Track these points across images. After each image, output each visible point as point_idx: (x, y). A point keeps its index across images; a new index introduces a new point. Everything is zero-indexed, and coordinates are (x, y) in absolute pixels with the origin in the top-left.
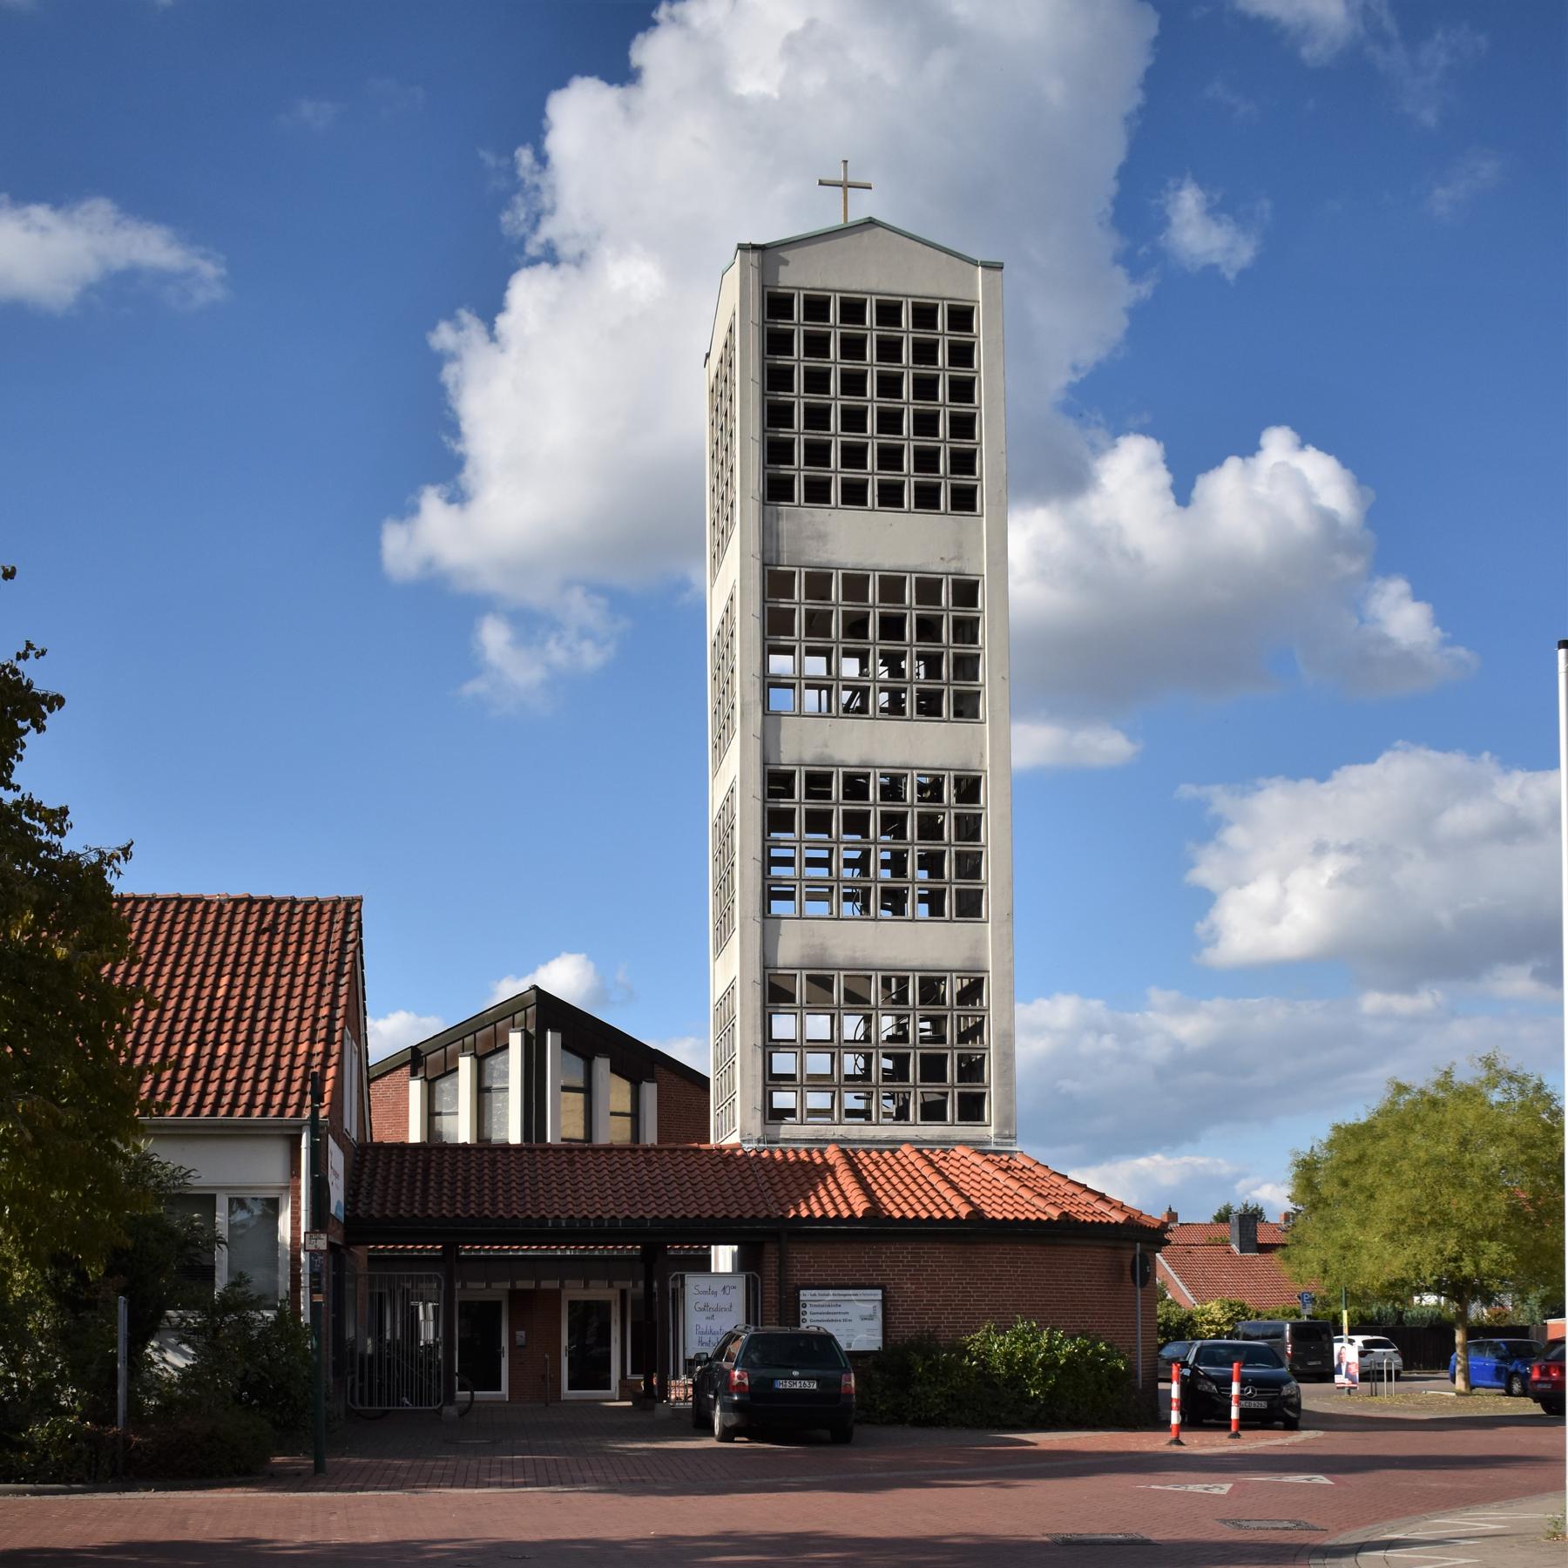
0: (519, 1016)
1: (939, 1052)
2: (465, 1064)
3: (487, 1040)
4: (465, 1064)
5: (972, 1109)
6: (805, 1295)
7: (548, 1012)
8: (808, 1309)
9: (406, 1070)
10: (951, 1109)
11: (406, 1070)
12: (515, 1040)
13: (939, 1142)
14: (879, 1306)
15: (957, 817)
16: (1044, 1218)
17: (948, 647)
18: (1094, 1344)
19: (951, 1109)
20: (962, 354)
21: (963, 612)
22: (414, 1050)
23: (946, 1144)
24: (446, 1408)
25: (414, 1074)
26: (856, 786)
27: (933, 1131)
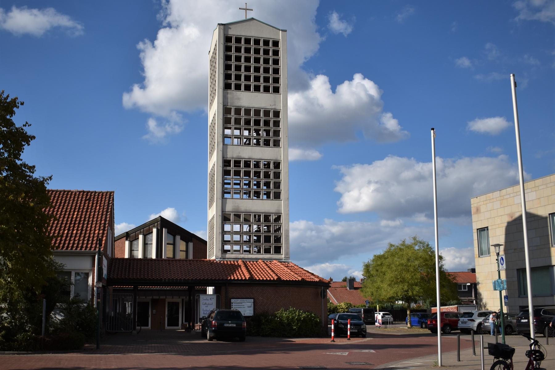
2: (141, 237)
4: (141, 237)
5: (278, 250)
7: (163, 223)
9: (125, 238)
10: (272, 250)
11: (125, 238)
19: (272, 250)
21: (276, 119)
25: (127, 239)
27: (267, 256)
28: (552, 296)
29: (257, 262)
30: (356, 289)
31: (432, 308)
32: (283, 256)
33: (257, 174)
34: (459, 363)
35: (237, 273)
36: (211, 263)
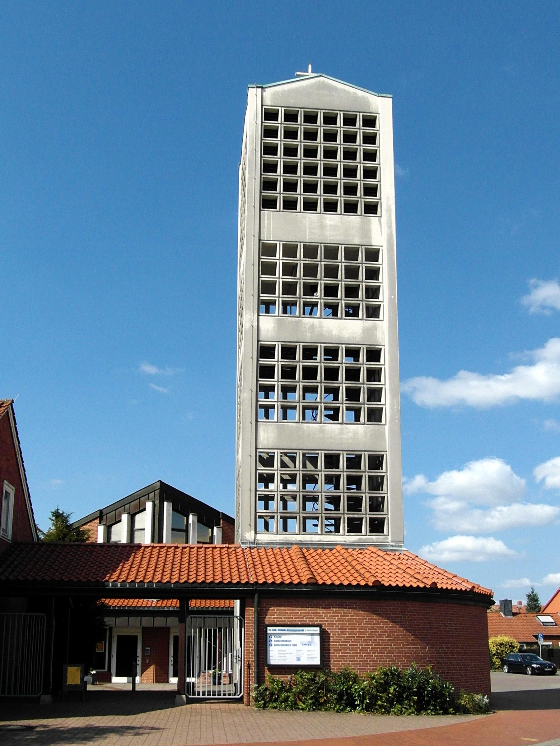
0: (151, 495)
1: (355, 491)
2: (125, 517)
3: (136, 506)
4: (125, 517)
5: (377, 526)
6: (270, 630)
7: (166, 492)
8: (273, 638)
9: (97, 521)
10: (365, 527)
11: (97, 521)
12: (149, 506)
13: (359, 545)
14: (317, 639)
15: (370, 477)
16: (422, 586)
17: (363, 364)
18: (432, 678)
19: (365, 527)
20: (377, 483)
21: (374, 473)
22: (101, 511)
23: (362, 546)
24: (43, 697)
25: (100, 523)
26: (332, 460)
27: (353, 538)
28: (381, 217)
29: (288, 549)
30: (514, 614)
31: (238, 601)
32: (390, 538)
33: (355, 481)
34: (295, 469)
35: (114, 603)
36: (237, 599)
